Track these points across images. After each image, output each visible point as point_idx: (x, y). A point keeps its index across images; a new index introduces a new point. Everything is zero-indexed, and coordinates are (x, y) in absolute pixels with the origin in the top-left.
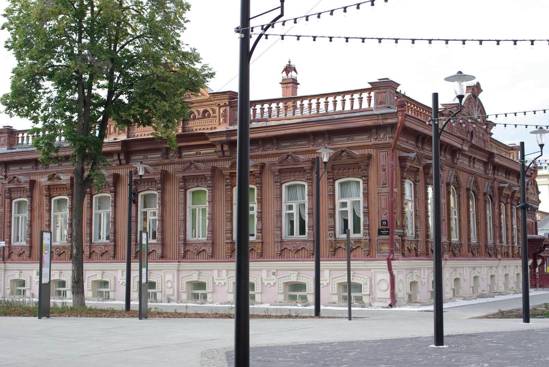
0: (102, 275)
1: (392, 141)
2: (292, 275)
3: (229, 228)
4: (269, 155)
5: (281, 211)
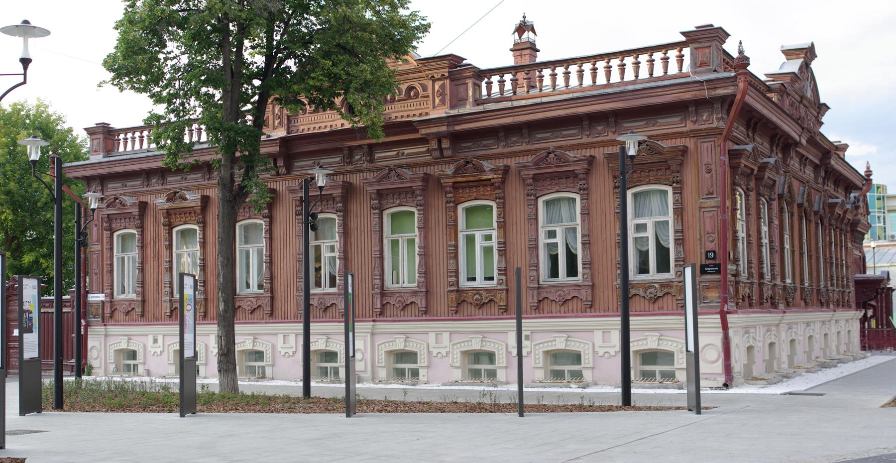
0: (327, 342)
1: (722, 124)
2: (558, 339)
3: (452, 268)
4: (515, 152)
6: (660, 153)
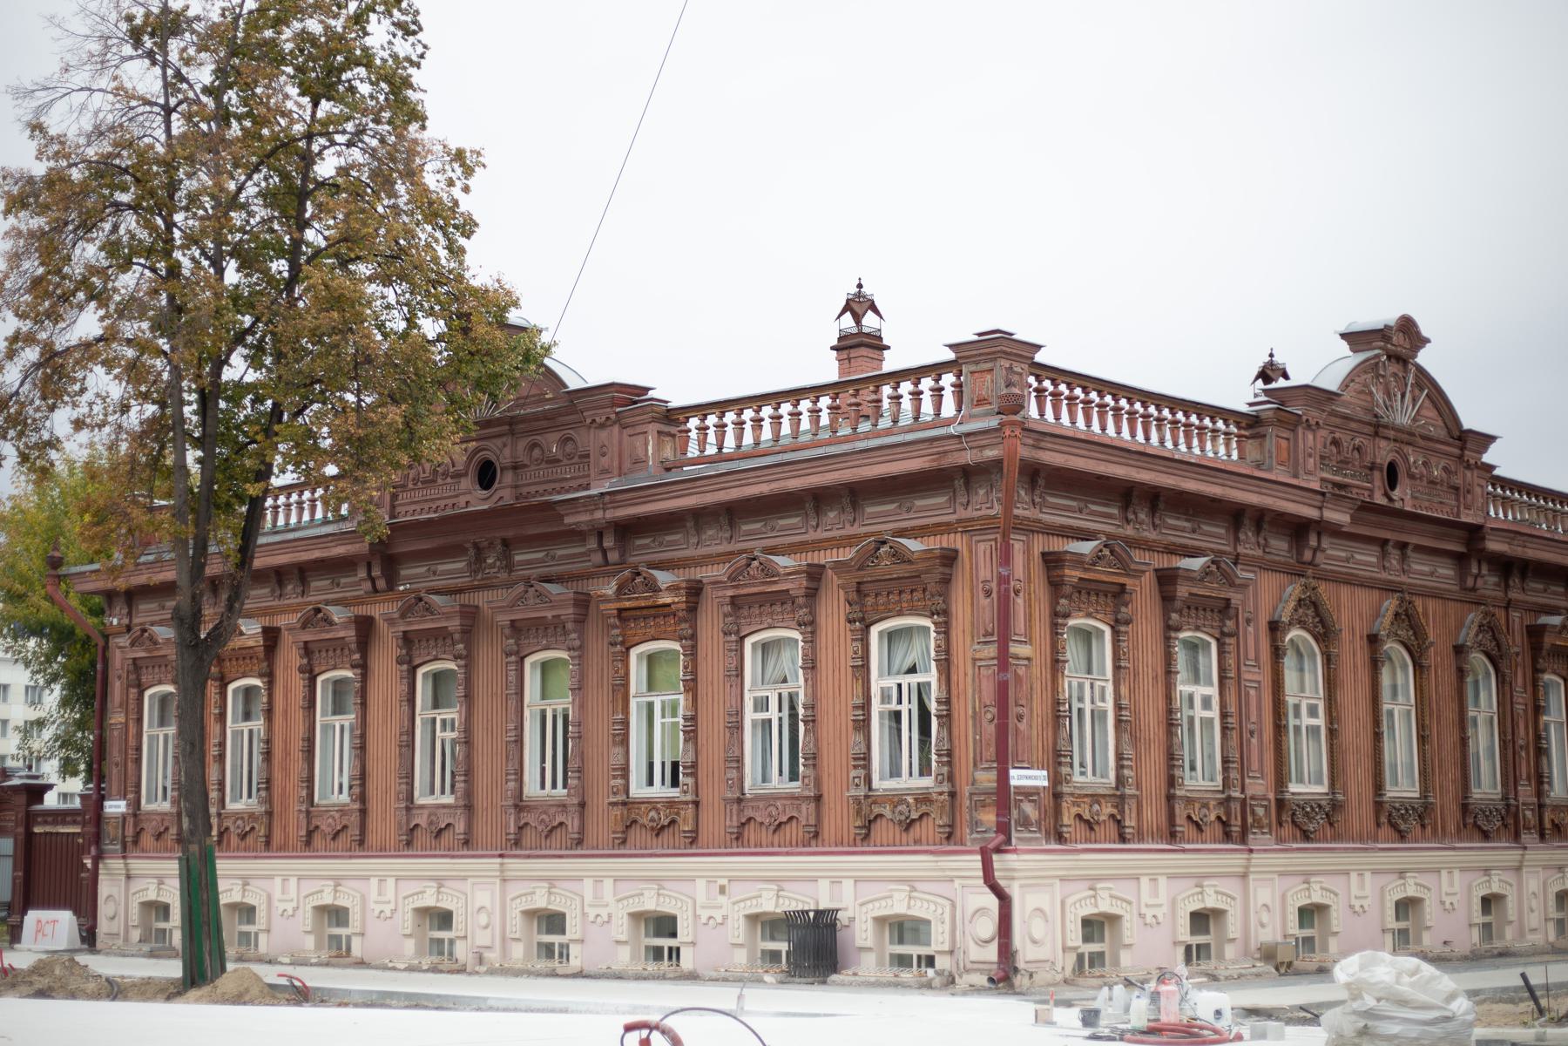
1: (997, 509)
2: (764, 893)
4: (710, 556)
5: (740, 713)
6: (910, 562)
